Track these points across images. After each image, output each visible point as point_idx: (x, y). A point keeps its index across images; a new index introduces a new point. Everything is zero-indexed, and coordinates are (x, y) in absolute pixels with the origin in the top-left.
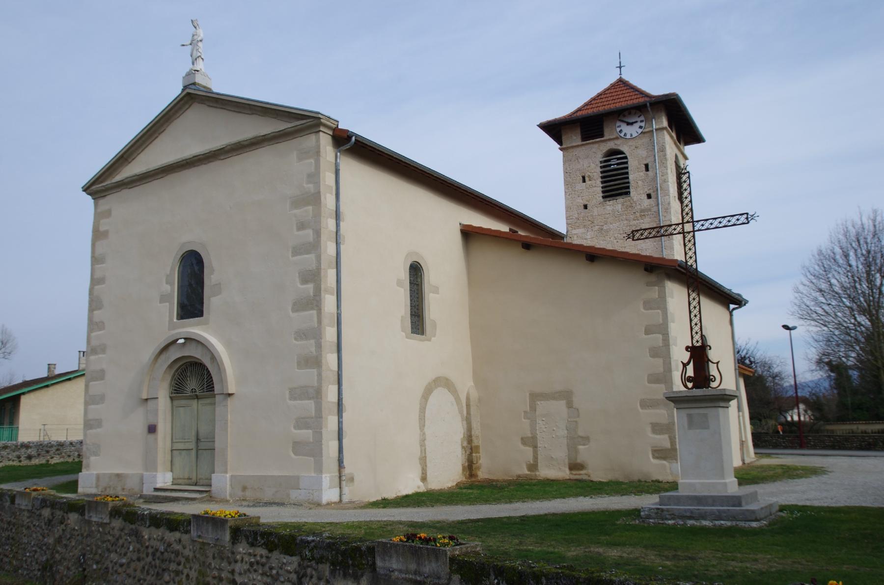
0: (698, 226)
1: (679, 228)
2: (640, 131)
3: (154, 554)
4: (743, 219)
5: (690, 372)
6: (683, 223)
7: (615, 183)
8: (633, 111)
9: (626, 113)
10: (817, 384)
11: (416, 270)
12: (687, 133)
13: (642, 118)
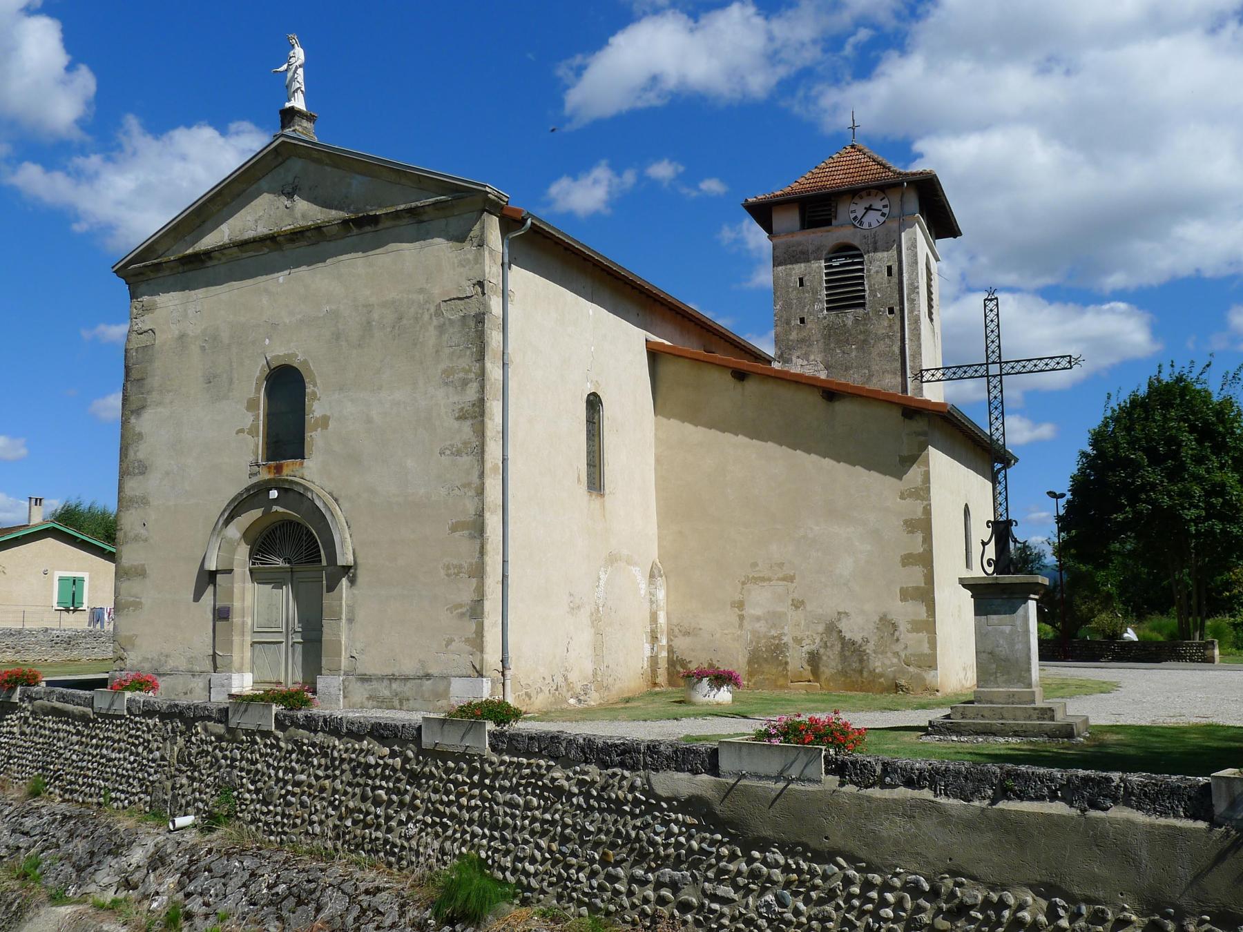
0: (1007, 368)
1: (982, 370)
2: (882, 219)
3: (353, 770)
4: (1064, 363)
5: (991, 552)
6: (987, 364)
7: (846, 293)
8: (873, 192)
9: (864, 193)
10: (110, 511)
11: (594, 403)
12: (942, 224)
13: (886, 202)
